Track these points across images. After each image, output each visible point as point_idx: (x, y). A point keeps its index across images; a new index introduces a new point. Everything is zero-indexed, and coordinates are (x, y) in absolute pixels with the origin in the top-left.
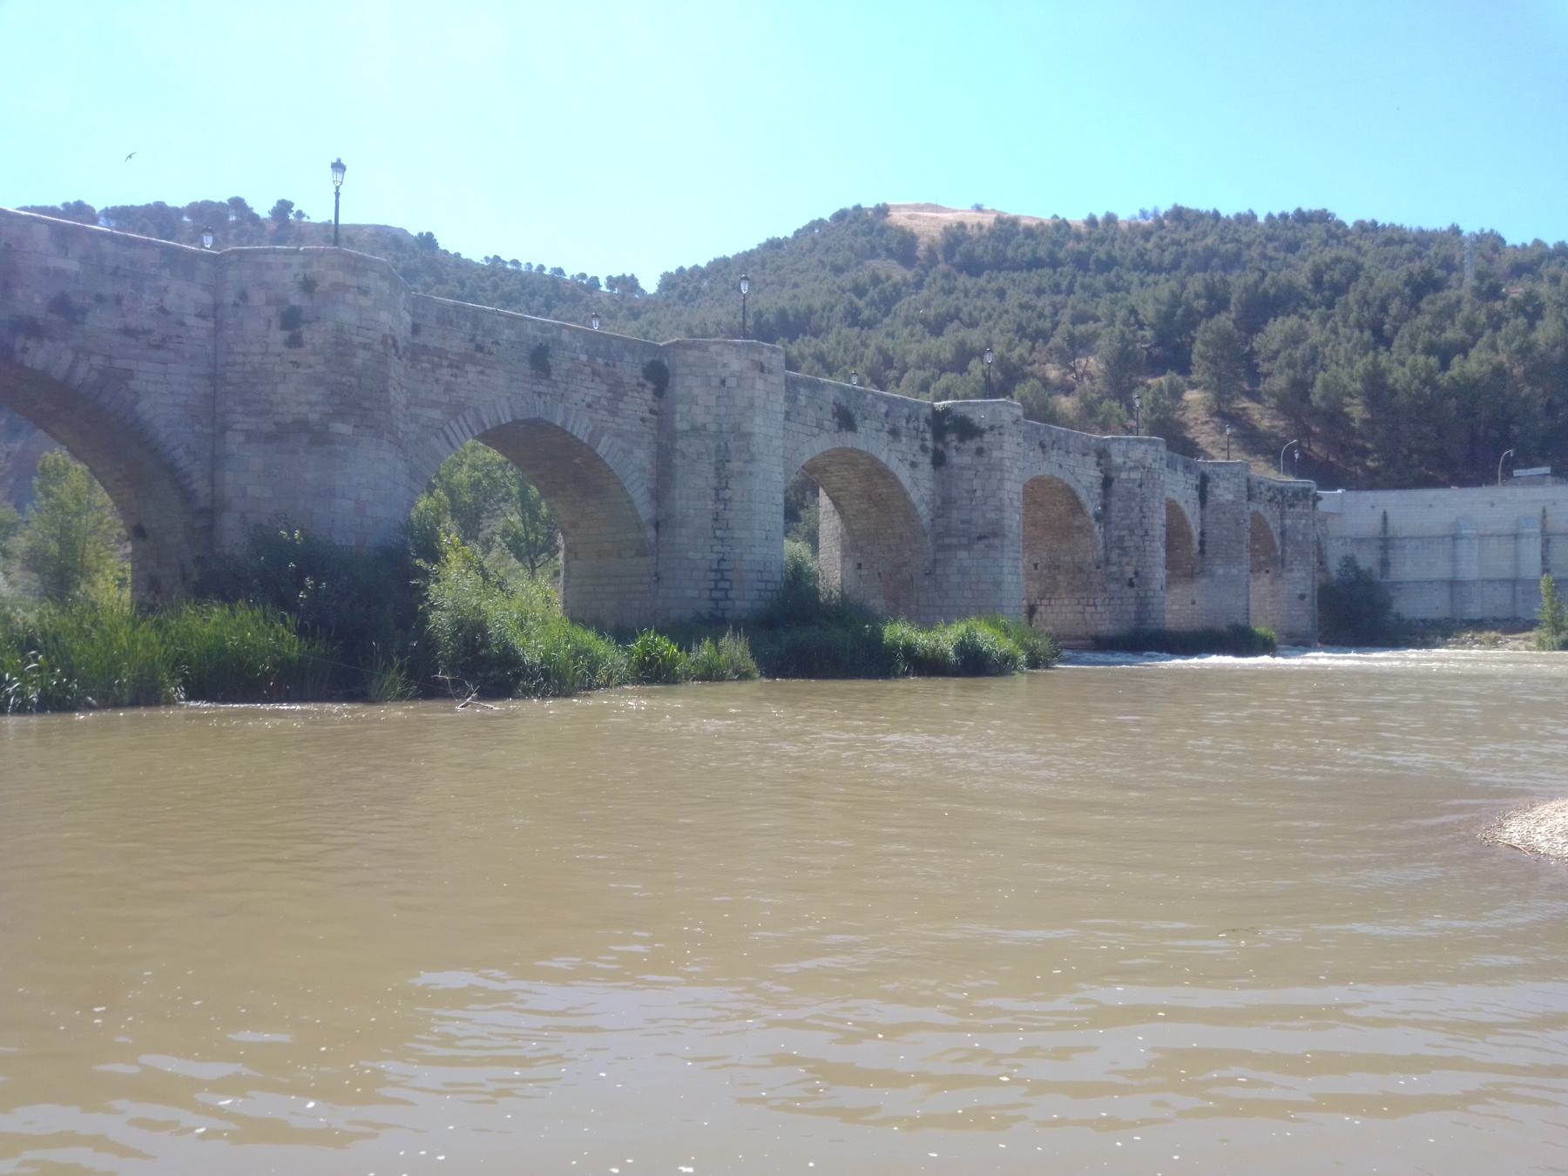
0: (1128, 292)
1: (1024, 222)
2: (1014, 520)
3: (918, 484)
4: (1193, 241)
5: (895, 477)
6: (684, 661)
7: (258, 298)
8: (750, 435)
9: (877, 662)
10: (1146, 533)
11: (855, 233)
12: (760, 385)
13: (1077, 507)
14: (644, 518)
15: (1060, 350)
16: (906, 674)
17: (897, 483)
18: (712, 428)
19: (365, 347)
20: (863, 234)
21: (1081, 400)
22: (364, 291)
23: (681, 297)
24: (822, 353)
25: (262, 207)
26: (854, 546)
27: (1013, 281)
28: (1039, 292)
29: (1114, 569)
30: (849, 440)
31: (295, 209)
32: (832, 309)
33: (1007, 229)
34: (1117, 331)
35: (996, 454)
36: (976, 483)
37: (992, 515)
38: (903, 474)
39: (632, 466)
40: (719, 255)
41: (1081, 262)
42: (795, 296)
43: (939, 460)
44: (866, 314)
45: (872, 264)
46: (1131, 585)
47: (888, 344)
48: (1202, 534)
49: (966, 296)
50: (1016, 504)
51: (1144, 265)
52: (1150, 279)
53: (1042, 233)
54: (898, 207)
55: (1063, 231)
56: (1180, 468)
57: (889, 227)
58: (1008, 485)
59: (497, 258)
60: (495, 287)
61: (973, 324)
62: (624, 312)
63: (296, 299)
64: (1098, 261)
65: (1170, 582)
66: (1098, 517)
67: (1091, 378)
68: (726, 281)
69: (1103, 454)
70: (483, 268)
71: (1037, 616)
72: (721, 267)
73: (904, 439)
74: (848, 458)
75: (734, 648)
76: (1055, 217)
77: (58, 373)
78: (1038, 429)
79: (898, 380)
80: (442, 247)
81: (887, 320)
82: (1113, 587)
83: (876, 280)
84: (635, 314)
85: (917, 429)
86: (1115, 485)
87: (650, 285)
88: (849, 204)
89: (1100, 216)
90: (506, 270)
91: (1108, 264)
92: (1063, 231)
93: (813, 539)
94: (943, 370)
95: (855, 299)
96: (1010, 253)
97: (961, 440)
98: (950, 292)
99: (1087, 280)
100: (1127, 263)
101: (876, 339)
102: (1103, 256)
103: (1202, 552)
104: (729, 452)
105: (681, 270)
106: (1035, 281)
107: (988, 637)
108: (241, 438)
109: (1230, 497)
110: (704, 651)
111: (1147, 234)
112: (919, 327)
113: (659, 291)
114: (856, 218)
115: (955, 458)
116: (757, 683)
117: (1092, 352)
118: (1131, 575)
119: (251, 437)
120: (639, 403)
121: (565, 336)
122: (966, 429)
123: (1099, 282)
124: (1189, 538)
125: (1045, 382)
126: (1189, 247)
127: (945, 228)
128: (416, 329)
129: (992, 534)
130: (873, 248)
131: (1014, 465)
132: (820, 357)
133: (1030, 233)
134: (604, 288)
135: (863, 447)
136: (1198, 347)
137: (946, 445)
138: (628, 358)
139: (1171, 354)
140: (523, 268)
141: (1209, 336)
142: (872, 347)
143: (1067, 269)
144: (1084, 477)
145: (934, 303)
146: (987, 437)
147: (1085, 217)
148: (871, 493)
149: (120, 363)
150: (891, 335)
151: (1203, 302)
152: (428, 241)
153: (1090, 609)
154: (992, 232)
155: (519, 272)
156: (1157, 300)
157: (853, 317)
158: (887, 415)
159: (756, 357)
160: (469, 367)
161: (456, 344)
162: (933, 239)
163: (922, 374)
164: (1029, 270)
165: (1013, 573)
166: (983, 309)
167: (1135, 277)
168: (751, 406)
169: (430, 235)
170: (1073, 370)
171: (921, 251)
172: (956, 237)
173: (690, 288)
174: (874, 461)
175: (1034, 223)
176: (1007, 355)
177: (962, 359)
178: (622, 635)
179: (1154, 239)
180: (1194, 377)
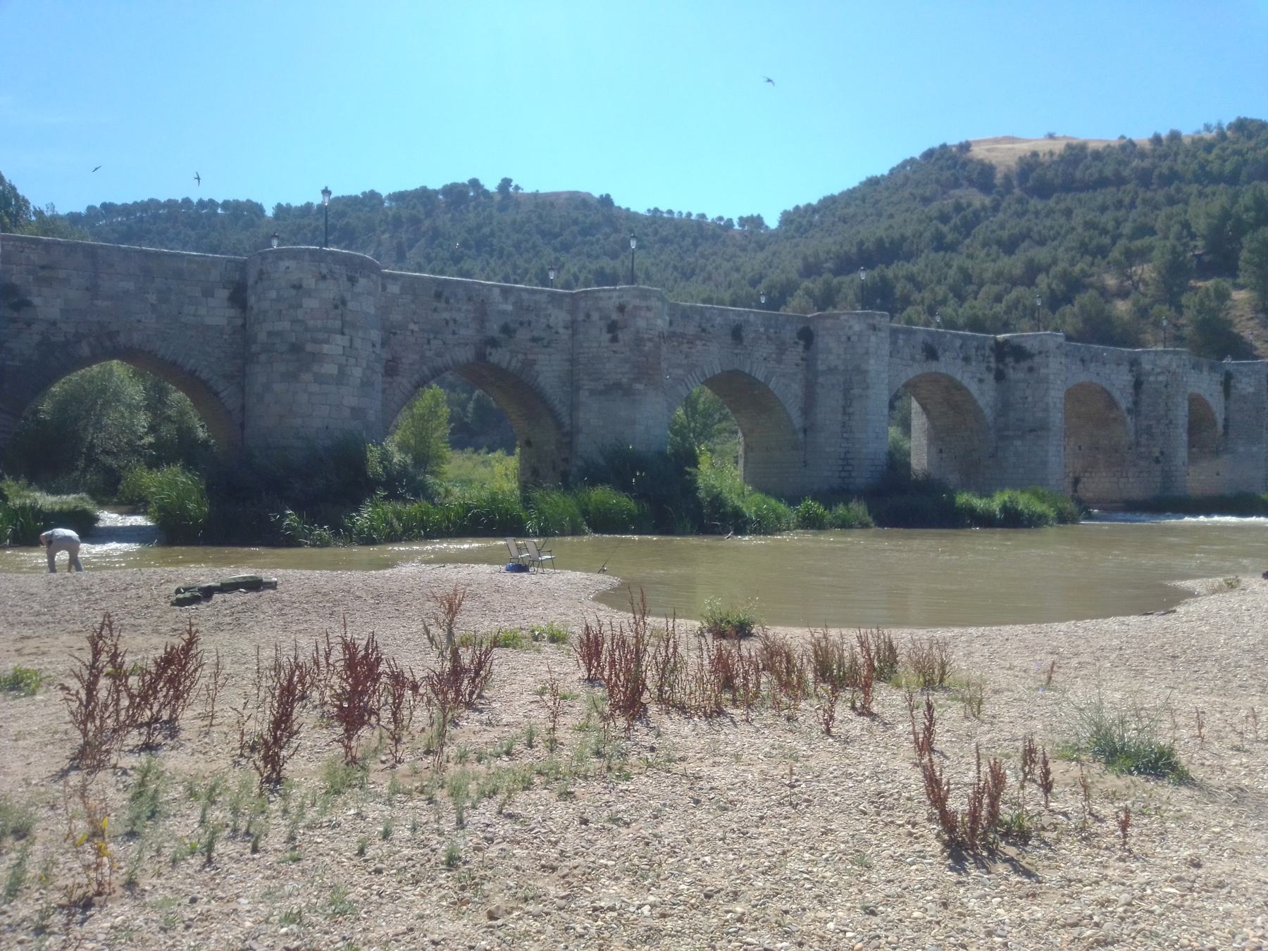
0: (1187, 203)
1: (1092, 146)
2: (1057, 418)
3: (983, 393)
4: (1254, 149)
5: (966, 389)
6: (828, 516)
7: (595, 316)
8: (867, 372)
9: (952, 518)
10: (1171, 422)
11: (941, 169)
12: (873, 339)
13: (1112, 404)
14: (797, 427)
15: (1117, 263)
16: (970, 526)
17: (969, 394)
18: (841, 368)
19: (650, 340)
20: (950, 167)
21: (1134, 305)
22: (649, 309)
23: (797, 230)
24: (912, 275)
25: (491, 185)
26: (937, 436)
27: (1080, 201)
28: (1103, 209)
29: (1143, 450)
30: (934, 367)
31: (513, 184)
32: (920, 236)
33: (1076, 154)
34: (1168, 244)
35: (1043, 371)
36: (1028, 392)
37: (1040, 415)
38: (973, 388)
39: (789, 391)
40: (828, 193)
41: (1145, 178)
42: (891, 226)
43: (1000, 376)
44: (950, 237)
45: (957, 192)
46: (1157, 461)
47: (969, 264)
48: (1226, 420)
49: (1037, 217)
50: (1059, 405)
51: (1205, 176)
52: (1208, 190)
53: (1109, 155)
54: (978, 142)
55: (1128, 150)
56: (1205, 369)
57: (971, 161)
58: (1053, 393)
59: (656, 210)
60: (656, 232)
61: (1042, 242)
62: (753, 245)
63: (615, 316)
64: (1161, 176)
65: (1193, 459)
66: (1129, 411)
67: (1146, 284)
68: (834, 215)
69: (1134, 363)
70: (647, 218)
71: (1080, 486)
72: (829, 203)
73: (974, 363)
74: (935, 378)
75: (858, 509)
76: (1123, 137)
77: (504, 365)
78: (1079, 348)
79: (976, 293)
80: (616, 204)
81: (968, 241)
82: (1142, 463)
83: (958, 208)
84: (761, 247)
85: (983, 356)
86: (1144, 386)
87: (772, 222)
88: (936, 144)
89: (1164, 134)
90: (664, 219)
91: (1172, 177)
92: (1128, 150)
93: (906, 426)
94: (1014, 284)
95: (941, 226)
96: (1078, 174)
97: (1017, 361)
98: (1024, 213)
99: (1149, 194)
100: (1189, 176)
101: (958, 261)
102: (1166, 171)
103: (1226, 433)
104: (852, 382)
105: (797, 208)
106: (1100, 199)
107: (1024, 501)
108: (587, 394)
109: (1251, 390)
110: (841, 510)
111: (1209, 147)
112: (995, 247)
113: (780, 226)
114: (942, 156)
115: (1012, 374)
116: (872, 530)
117: (1150, 261)
118: (1158, 454)
119: (592, 392)
120: (795, 354)
121: (752, 318)
122: (1020, 353)
123: (1160, 196)
124: (1215, 423)
125: (1103, 291)
126: (1250, 156)
127: (1020, 158)
128: (671, 323)
129: (1039, 429)
130: (957, 179)
131: (1058, 376)
132: (911, 278)
133: (1097, 155)
134: (737, 227)
135: (943, 371)
136: (1244, 254)
137: (1006, 365)
138: (789, 327)
139: (1221, 261)
140: (676, 216)
141: (1254, 245)
142: (955, 268)
143: (1129, 187)
144: (1119, 381)
145: (1008, 226)
146: (1037, 359)
147: (1151, 135)
148: (949, 404)
149: (531, 357)
150: (970, 256)
151: (1252, 214)
152: (606, 201)
153: (1122, 480)
154: (1062, 158)
155: (672, 219)
156: (1209, 215)
157: (940, 244)
158: (961, 347)
159: (871, 321)
160: (698, 342)
161: (691, 330)
162: (1009, 167)
163: (996, 289)
164: (1095, 189)
165: (1058, 456)
166: (1052, 228)
167: (1194, 188)
168: (867, 353)
169: (608, 196)
170: (1130, 278)
171: (999, 178)
172: (1030, 166)
173: (805, 222)
174: (951, 379)
175: (1100, 146)
176: (1070, 269)
177: (1031, 274)
178: (793, 501)
179: (1216, 151)
180: (1240, 280)
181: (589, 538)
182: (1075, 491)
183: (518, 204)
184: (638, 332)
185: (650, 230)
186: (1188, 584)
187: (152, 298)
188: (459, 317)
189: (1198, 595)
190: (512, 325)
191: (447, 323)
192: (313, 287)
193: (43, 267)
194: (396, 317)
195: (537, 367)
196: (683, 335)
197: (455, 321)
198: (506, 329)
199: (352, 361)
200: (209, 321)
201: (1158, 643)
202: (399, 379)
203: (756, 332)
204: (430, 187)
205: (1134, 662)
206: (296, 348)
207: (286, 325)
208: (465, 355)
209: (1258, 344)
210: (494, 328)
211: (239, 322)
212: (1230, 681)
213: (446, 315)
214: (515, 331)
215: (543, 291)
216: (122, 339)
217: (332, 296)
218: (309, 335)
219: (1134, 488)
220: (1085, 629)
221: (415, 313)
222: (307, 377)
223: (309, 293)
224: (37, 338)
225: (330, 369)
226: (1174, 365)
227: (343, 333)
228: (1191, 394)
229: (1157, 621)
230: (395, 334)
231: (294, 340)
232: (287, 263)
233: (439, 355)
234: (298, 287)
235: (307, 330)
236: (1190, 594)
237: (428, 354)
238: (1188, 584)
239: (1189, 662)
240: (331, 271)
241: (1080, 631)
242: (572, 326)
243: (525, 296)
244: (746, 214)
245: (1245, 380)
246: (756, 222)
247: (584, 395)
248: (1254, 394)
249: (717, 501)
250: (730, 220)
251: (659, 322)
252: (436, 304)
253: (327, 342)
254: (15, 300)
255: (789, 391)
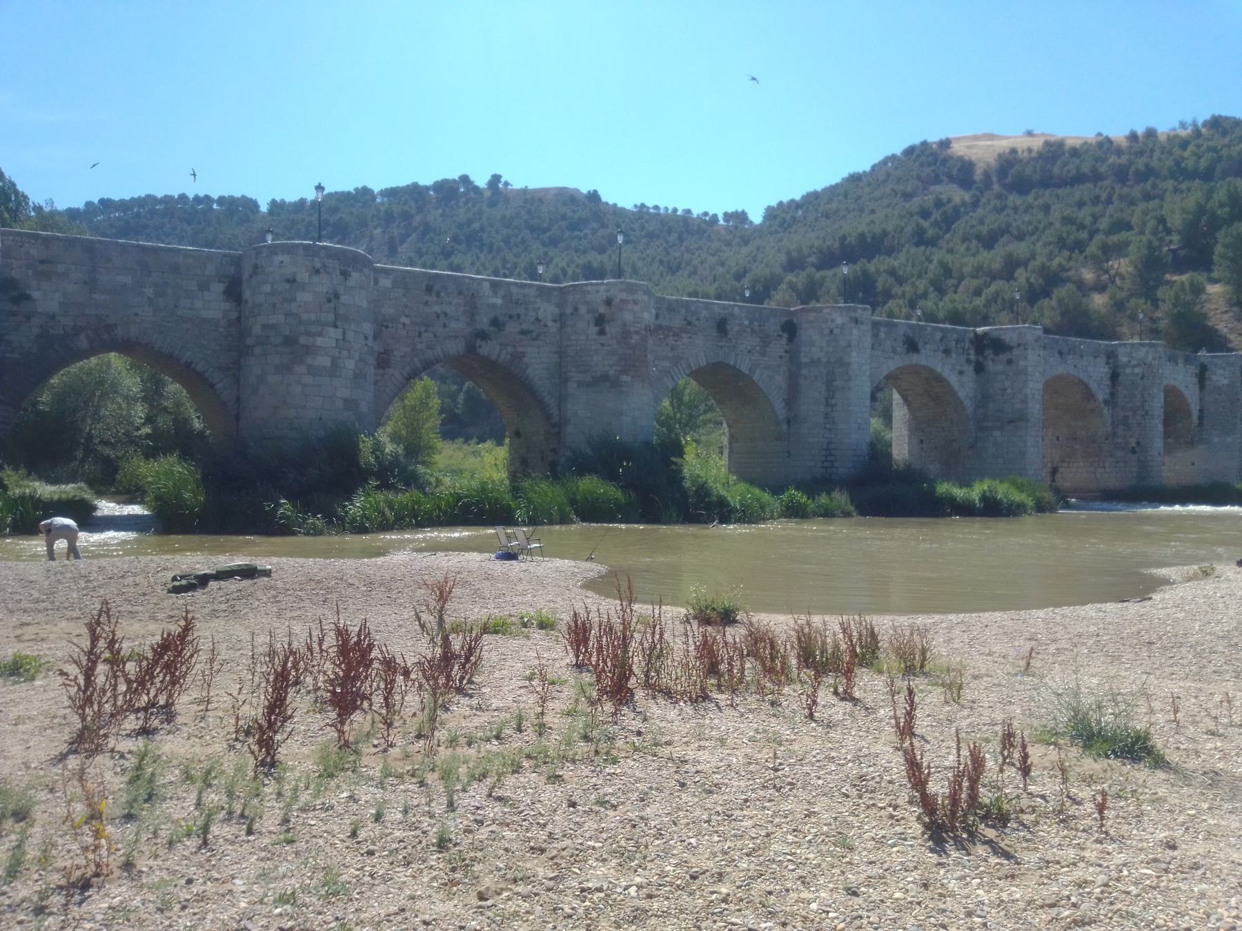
0: (1162, 199)
1: (1069, 143)
2: (1035, 409)
3: (963, 385)
4: (1228, 146)
5: (946, 381)
6: (811, 505)
7: (583, 309)
8: (849, 364)
9: (932, 507)
10: (1147, 413)
11: (922, 165)
12: (855, 332)
13: (1089, 395)
14: (781, 418)
15: (1094, 258)
16: (950, 515)
17: (949, 386)
18: (824, 360)
19: (637, 333)
20: (930, 163)
21: (1111, 298)
22: (635, 302)
23: (781, 225)
24: (894, 269)
25: (481, 181)
26: (918, 427)
27: (1058, 196)
28: (1081, 204)
29: (1119, 440)
30: (915, 359)
31: (503, 180)
32: (902, 231)
33: (1054, 151)
34: (1144, 239)
35: (1021, 363)
36: (1007, 384)
37: (1018, 406)
38: (953, 380)
39: (772, 383)
40: (811, 189)
41: (1121, 174)
42: (872, 222)
43: (979, 368)
44: (930, 232)
45: (937, 188)
46: (1133, 451)
47: (949, 258)
48: (1201, 411)
49: (1016, 213)
50: (1037, 397)
51: (1181, 173)
52: (1184, 186)
53: (1086, 152)
54: (958, 139)
55: (1105, 147)
56: (1180, 361)
57: (951, 157)
58: (1031, 385)
59: (643, 205)
60: (642, 227)
61: (1020, 237)
62: (737, 240)
63: (602, 310)
64: (1137, 172)
65: (1168, 450)
66: (1106, 402)
67: (1123, 278)
68: (816, 210)
69: (1111, 355)
70: (633, 213)
71: (1058, 475)
72: (812, 199)
73: (954, 356)
74: (915, 370)
75: (841, 498)
76: (1100, 134)
77: (494, 358)
78: (1057, 341)
79: (956, 287)
80: (604, 199)
81: (948, 236)
82: (1119, 453)
83: (939, 203)
84: (746, 241)
85: (963, 348)
86: (1121, 378)
87: (756, 217)
88: (916, 141)
89: (1140, 131)
90: (650, 214)
91: (1148, 173)
92: (1105, 147)
93: (887, 417)
94: (993, 278)
95: (922, 221)
96: (1056, 171)
97: (996, 354)
98: (1003, 208)
99: (1125, 190)
100: (1165, 172)
101: (938, 255)
102: (1142, 168)
103: (1201, 424)
104: (834, 374)
105: (781, 203)
106: (1077, 195)
107: (1003, 491)
108: (575, 385)
109: (1226, 382)
110: (823, 499)
111: (1184, 144)
112: (974, 242)
113: (764, 222)
114: (923, 152)
115: (991, 367)
116: (854, 519)
117: (1126, 256)
118: (1134, 445)
119: (580, 384)
120: (779, 346)
121: (736, 311)
122: (999, 346)
123: (1136, 191)
124: (1190, 414)
125: (1080, 285)
126: (1224, 152)
127: (999, 155)
128: (657, 316)
129: (1018, 420)
130: (937, 176)
131: (1036, 368)
132: (892, 273)
133: (1075, 152)
134: (722, 222)
135: (924, 363)
136: (1219, 249)
137: (985, 357)
138: (772, 320)
139: (1196, 255)
140: (662, 211)
141: (1229, 240)
142: (935, 262)
143: (1106, 183)
144: (1096, 373)
145: (987, 221)
146: (1016, 352)
147: (1127, 133)
148: (930, 395)
149: (520, 349)
150: (950, 251)
151: (1227, 209)
152: (594, 197)
153: (1099, 470)
154: (1041, 155)
155: (659, 214)
156: (1184, 211)
157: (921, 239)
158: (941, 340)
159: (853, 315)
160: (684, 335)
161: (677, 323)
162: (988, 164)
163: (975, 283)
164: (1072, 185)
165: (1036, 447)
166: (1030, 223)
167: (1170, 184)
168: (849, 346)
169: (595, 192)
170: (1107, 272)
171: (978, 175)
172: (1008, 163)
173: (788, 218)
174: (932, 371)
175: (1078, 143)
176: (1048, 264)
177: (1010, 268)
178: (777, 490)
179: (1191, 148)
180: (1215, 275)
181: (577, 527)
182: (1053, 481)
183: (507, 200)
184: (625, 325)
185: (636, 226)
186: (1163, 572)
187: (149, 292)
188: (450, 310)
189: (1174, 583)
190: (501, 318)
191: (438, 316)
192: (307, 281)
193: (42, 262)
194: (388, 310)
195: (526, 360)
196: (669, 328)
197: (446, 314)
198: (495, 322)
199: (345, 353)
200: (205, 314)
201: (1134, 629)
202: (391, 371)
203: (740, 325)
204: (422, 183)
205: (1111, 648)
206: (290, 341)
207: (280, 318)
208: (455, 347)
209: (1232, 337)
210: (484, 321)
211: (234, 315)
212: (1204, 667)
213: (437, 309)
214: (504, 324)
215: (532, 285)
216: (119, 332)
217: (325, 290)
218: (303, 328)
219: (1111, 478)
220: (1063, 616)
221: (406, 306)
222: (301, 369)
223: (302, 287)
224: (36, 331)
225: (324, 361)
226: (1150, 357)
227: (336, 326)
228: (1167, 386)
229: (1133, 608)
230: (387, 327)
231: (288, 333)
232: (281, 258)
233: (430, 347)
234: (291, 281)
235: (300, 323)
236: (1166, 582)
237: (419, 346)
238: (1163, 572)
239: (1164, 648)
240: (324, 265)
241: (1058, 618)
242: (561, 319)
243: (514, 290)
244: (730, 210)
245: (1219, 372)
246: (741, 217)
247: (572, 387)
248: (1228, 386)
249: (703, 490)
250: (715, 216)
251: (646, 315)
252: (427, 298)
253: (320, 334)
254: (15, 294)
255: (772, 383)
